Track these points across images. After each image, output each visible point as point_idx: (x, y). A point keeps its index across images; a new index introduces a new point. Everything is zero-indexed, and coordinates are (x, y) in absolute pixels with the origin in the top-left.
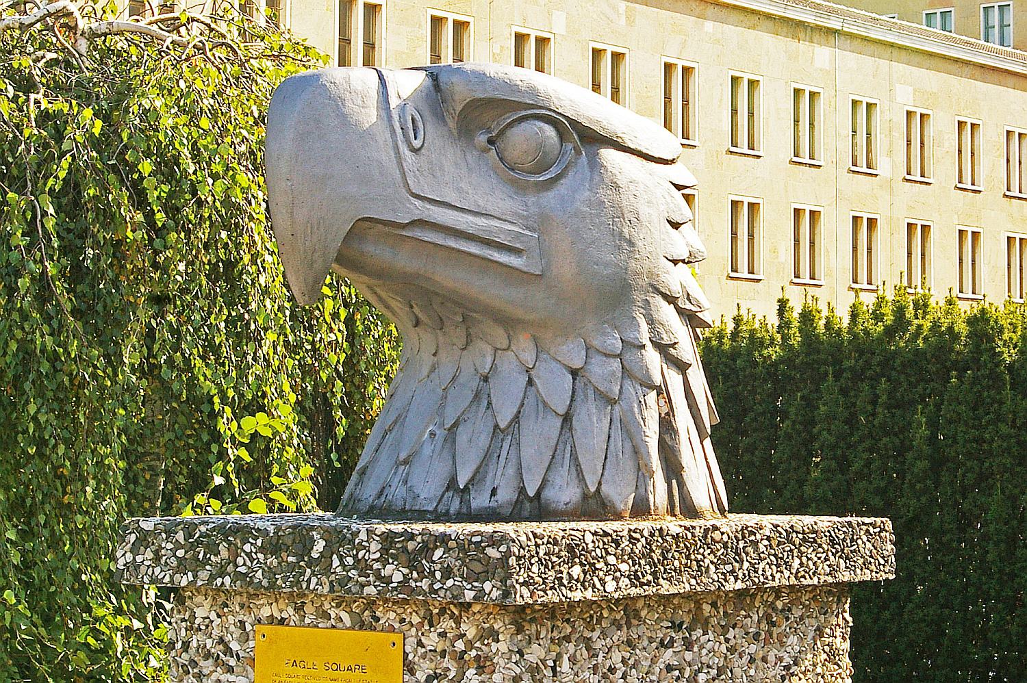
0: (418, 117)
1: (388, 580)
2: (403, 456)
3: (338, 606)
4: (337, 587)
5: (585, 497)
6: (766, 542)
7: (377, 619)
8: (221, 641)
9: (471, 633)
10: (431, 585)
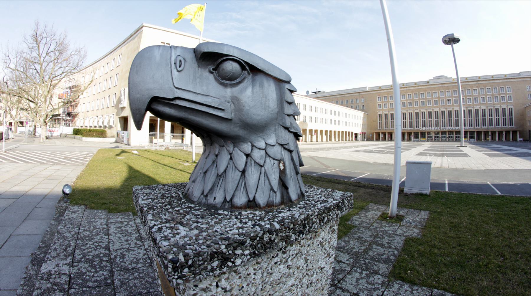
5: (249, 201)
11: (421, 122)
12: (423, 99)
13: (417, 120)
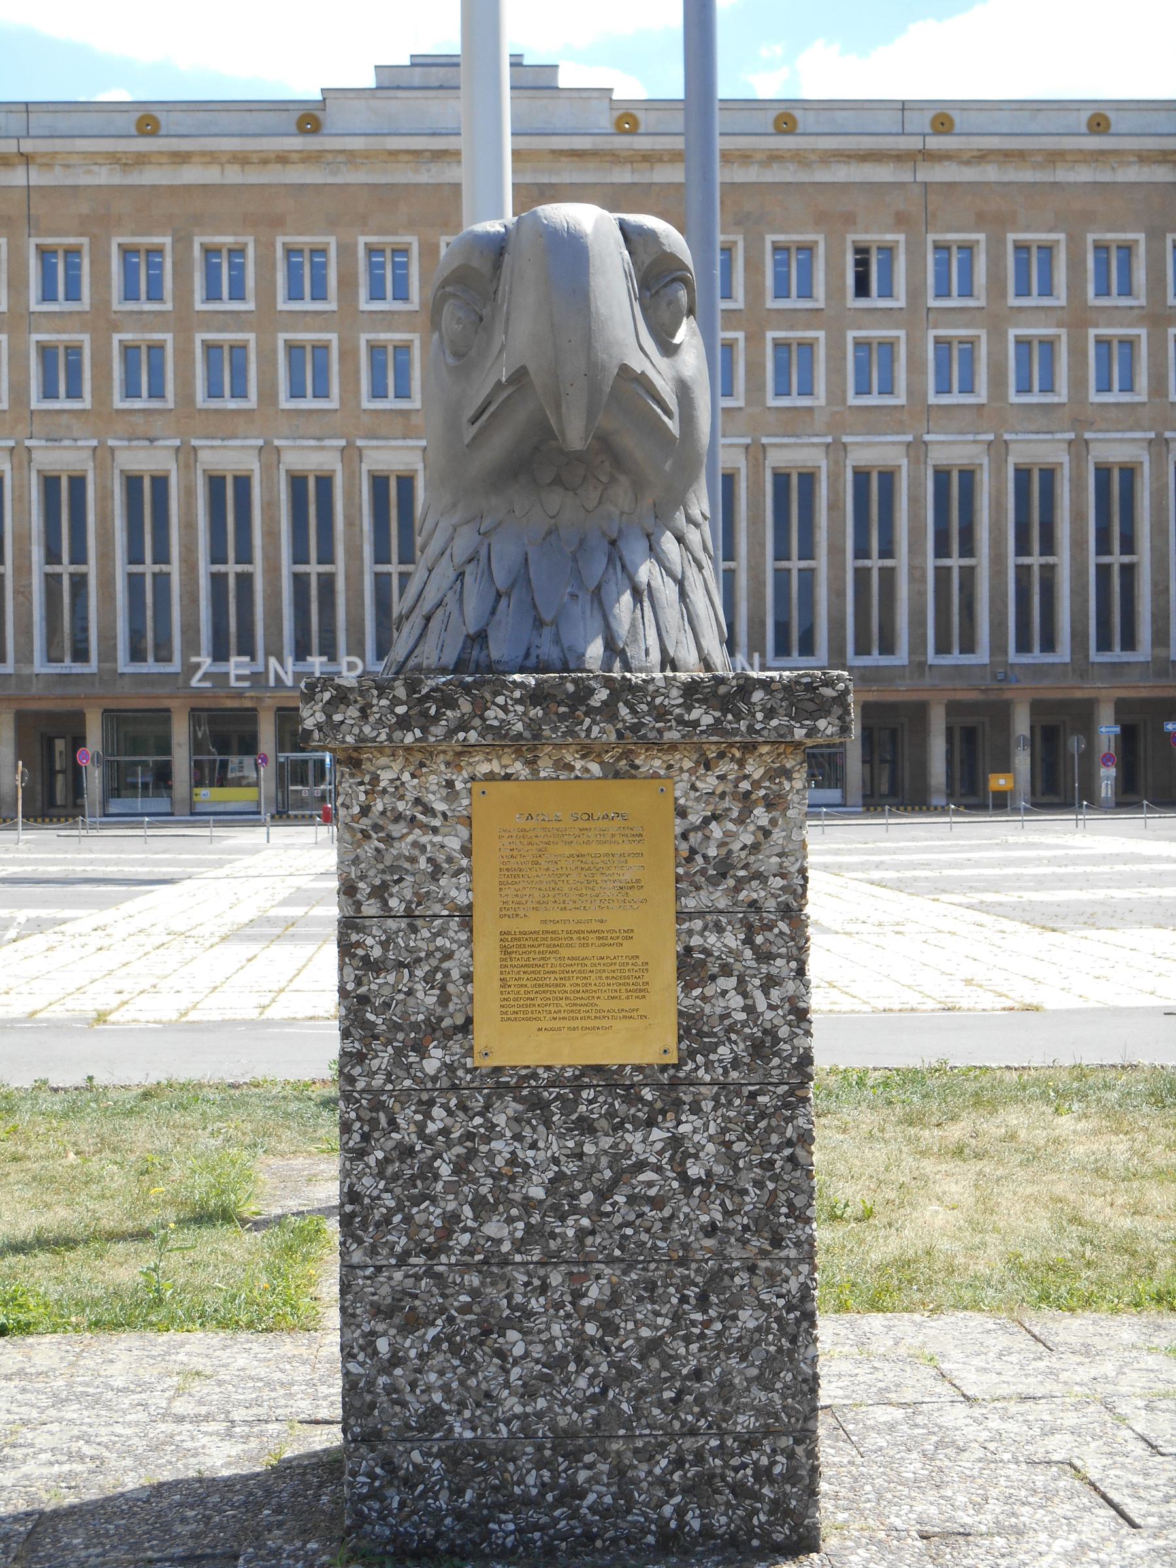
1: (696, 724)
8: (418, 801)
11: (191, 598)
12: (237, 320)
13: (149, 568)
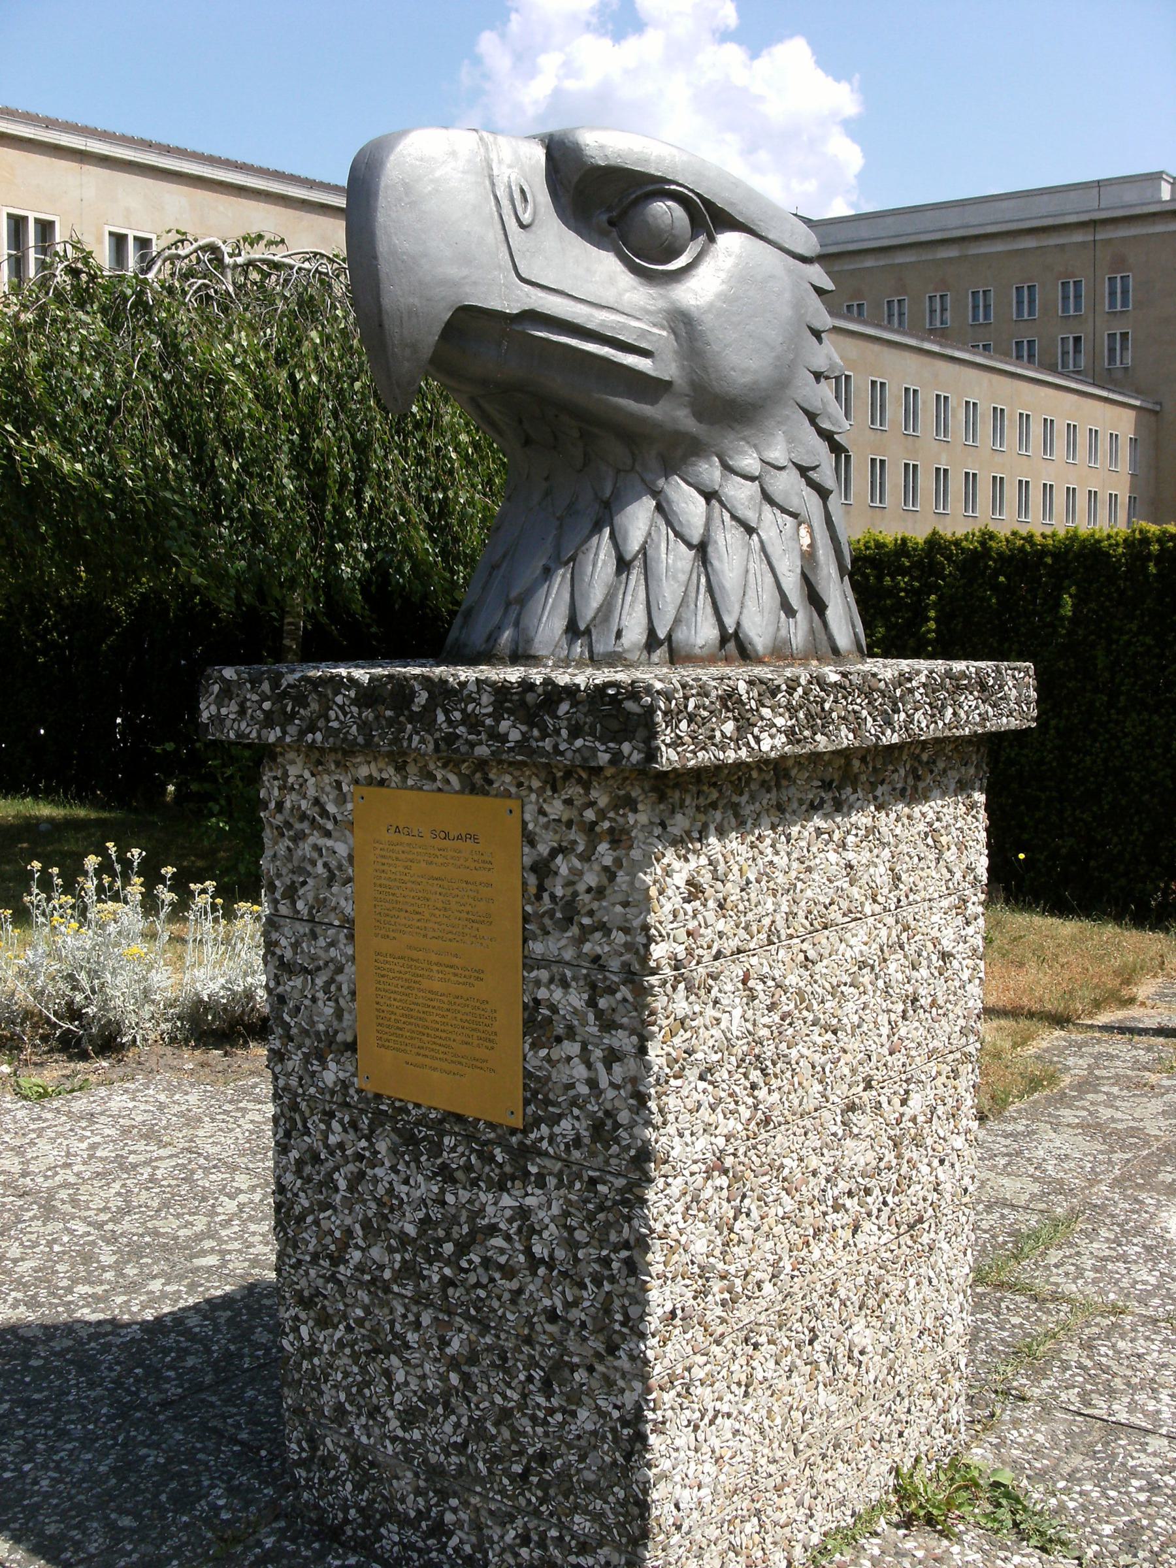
0: (526, 188)
2: (514, 594)
3: (445, 766)
4: (442, 745)
6: (922, 690)
7: (490, 782)
8: (317, 802)
9: (603, 801)
10: (556, 746)
